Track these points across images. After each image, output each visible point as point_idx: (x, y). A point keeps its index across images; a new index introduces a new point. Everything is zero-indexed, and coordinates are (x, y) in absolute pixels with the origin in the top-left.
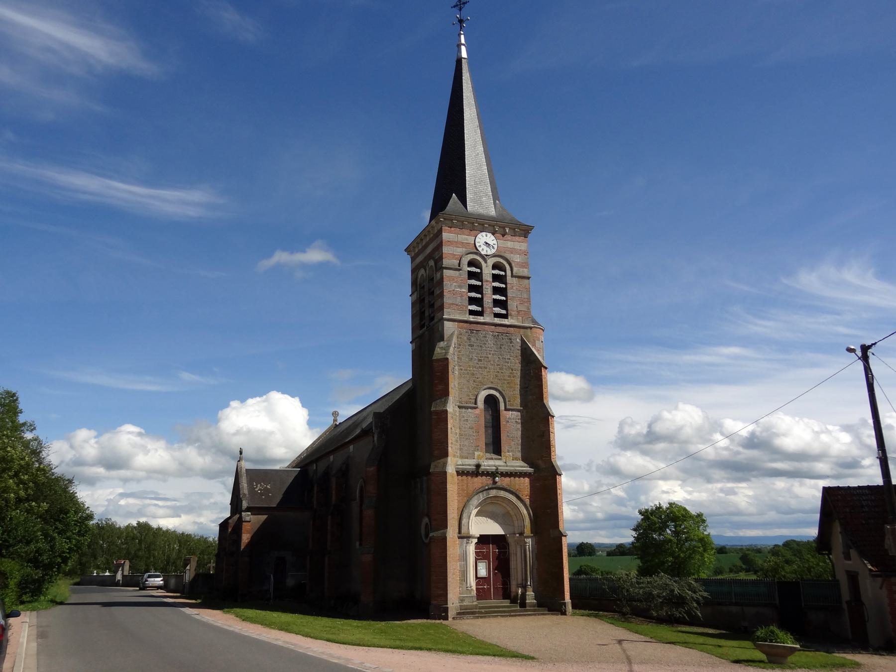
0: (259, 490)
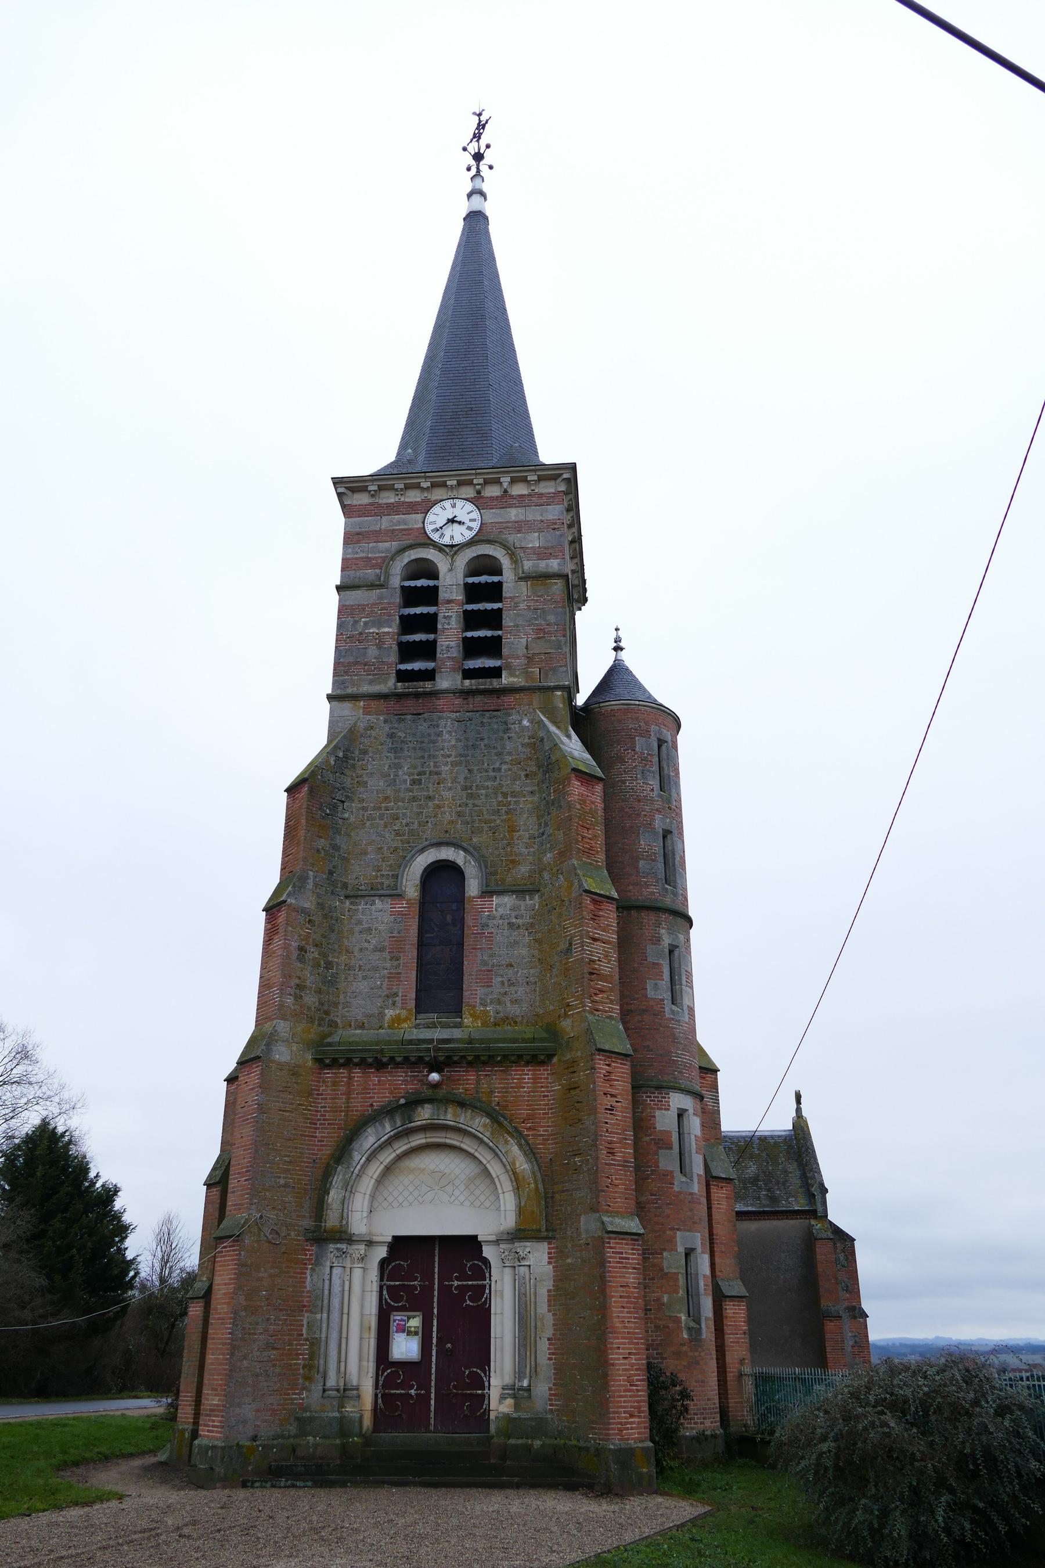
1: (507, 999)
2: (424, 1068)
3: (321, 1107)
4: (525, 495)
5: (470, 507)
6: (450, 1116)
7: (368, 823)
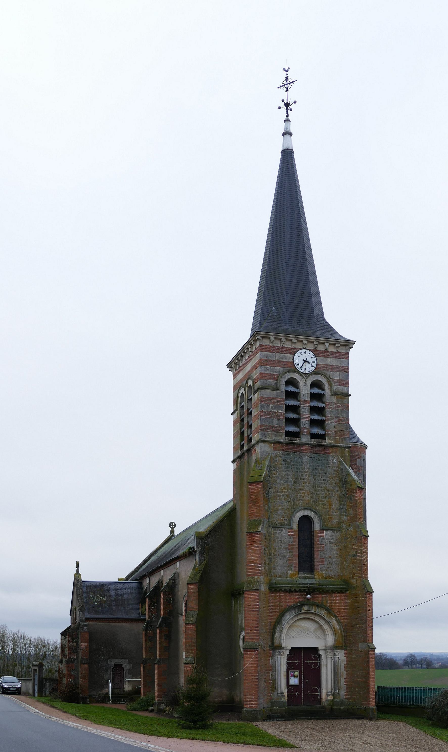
0: (95, 602)
1: (329, 569)
2: (305, 593)
3: (271, 605)
4: (333, 352)
5: (312, 355)
6: (313, 610)
7: (278, 498)
